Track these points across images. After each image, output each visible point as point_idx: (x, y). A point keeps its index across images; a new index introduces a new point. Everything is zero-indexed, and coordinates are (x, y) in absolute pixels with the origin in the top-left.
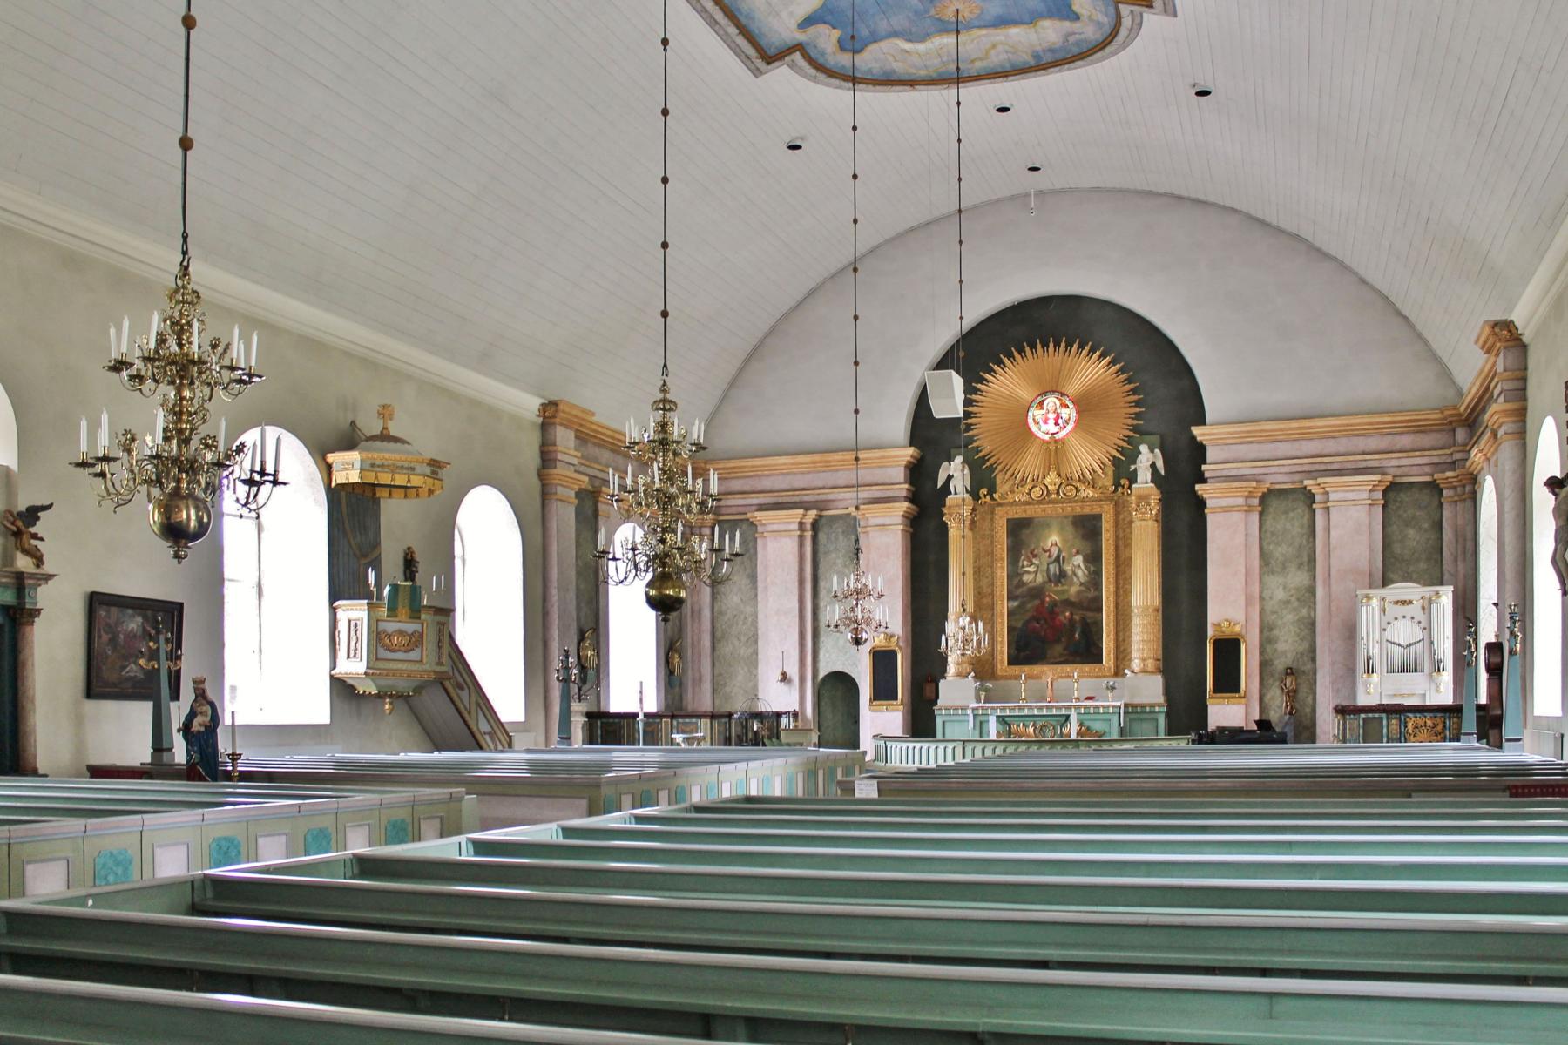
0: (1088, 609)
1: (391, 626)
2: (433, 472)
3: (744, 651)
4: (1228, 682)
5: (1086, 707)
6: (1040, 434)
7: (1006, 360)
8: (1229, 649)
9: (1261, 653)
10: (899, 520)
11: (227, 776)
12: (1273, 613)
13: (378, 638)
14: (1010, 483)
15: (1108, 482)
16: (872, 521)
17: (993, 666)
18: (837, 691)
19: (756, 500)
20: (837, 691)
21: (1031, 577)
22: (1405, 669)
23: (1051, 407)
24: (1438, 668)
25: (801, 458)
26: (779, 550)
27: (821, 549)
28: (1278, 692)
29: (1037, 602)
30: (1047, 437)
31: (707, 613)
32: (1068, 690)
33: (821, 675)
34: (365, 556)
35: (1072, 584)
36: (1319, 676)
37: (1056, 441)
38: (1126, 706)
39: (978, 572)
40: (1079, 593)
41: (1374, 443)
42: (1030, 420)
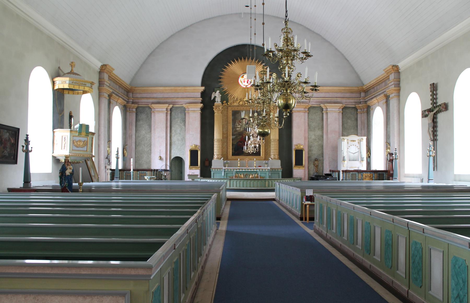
1: (77, 139)
2: (91, 86)
4: (299, 162)
5: (259, 169)
6: (242, 86)
7: (233, 62)
8: (299, 153)
9: (308, 154)
10: (199, 109)
11: (76, 190)
13: (73, 143)
16: (191, 109)
19: (151, 101)
21: (239, 129)
25: (167, 88)
26: (159, 118)
27: (173, 117)
28: (313, 166)
29: (241, 137)
30: (245, 87)
31: (134, 136)
33: (172, 157)
34: (61, 114)
37: (247, 88)
41: (339, 95)
42: (239, 81)
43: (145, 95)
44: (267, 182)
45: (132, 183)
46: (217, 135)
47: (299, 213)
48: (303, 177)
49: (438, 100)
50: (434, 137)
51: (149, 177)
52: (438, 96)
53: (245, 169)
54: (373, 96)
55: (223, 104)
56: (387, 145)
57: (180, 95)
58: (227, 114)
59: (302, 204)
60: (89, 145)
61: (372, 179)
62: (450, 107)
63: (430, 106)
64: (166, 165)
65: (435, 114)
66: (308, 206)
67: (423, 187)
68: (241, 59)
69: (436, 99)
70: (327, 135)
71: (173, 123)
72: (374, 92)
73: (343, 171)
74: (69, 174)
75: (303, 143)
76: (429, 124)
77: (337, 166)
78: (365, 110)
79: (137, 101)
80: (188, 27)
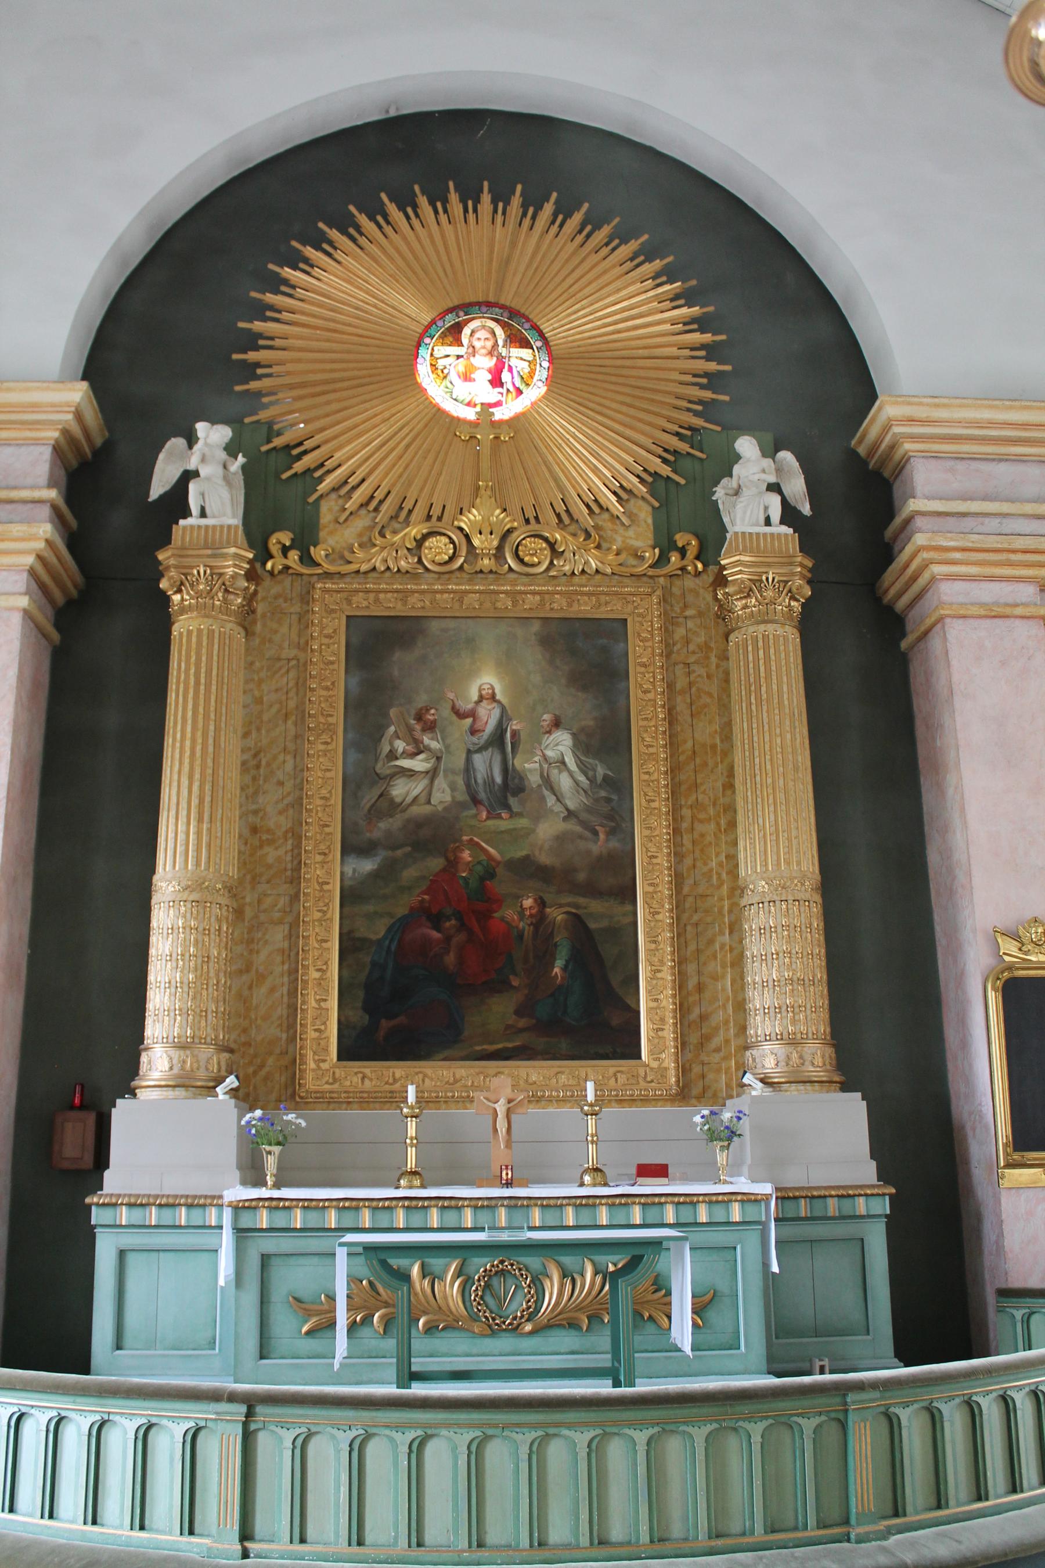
0: (591, 890)
10: (20, 581)
14: (361, 523)
15: (640, 536)
17: (292, 1067)
21: (417, 788)
29: (435, 864)
30: (470, 414)
32: (537, 1144)
35: (540, 814)
37: (495, 424)
38: (785, 1196)
39: (254, 766)
40: (561, 839)
44: (864, 1441)
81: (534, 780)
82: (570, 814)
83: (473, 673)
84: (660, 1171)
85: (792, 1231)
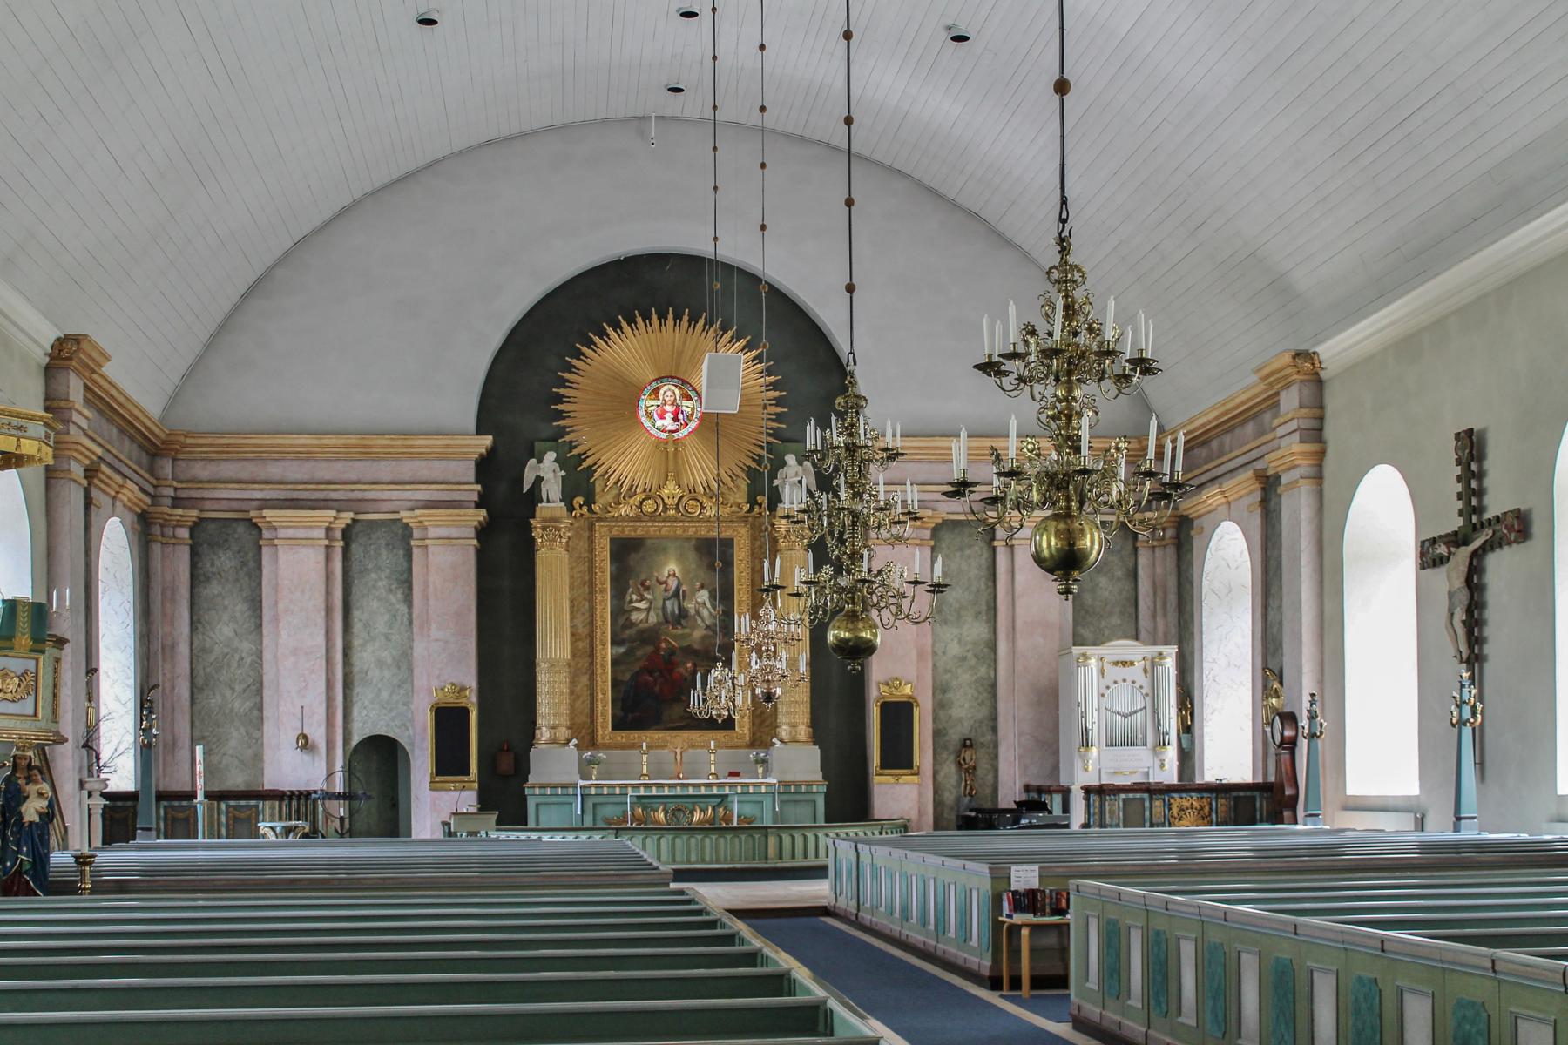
3: (240, 705)
4: (898, 756)
5: (733, 786)
6: (653, 431)
8: (898, 715)
11: (66, 888)
12: (947, 671)
14: (615, 492)
15: (740, 496)
18: (379, 759)
20: (379, 759)
21: (642, 616)
22: (1126, 742)
23: (669, 397)
24: (1161, 743)
25: (327, 440)
26: (297, 566)
27: (355, 567)
29: (650, 649)
30: (663, 436)
31: (183, 649)
33: (356, 740)
35: (694, 627)
36: (1002, 750)
40: (704, 638)
42: (642, 413)
43: (228, 470)
44: (772, 841)
45: (201, 851)
46: (553, 645)
47: (984, 964)
48: (913, 815)
49: (1487, 500)
50: (1471, 648)
51: (279, 825)
52: (1487, 482)
53: (670, 786)
54: (1203, 479)
55: (571, 509)
56: (1265, 679)
57: (385, 470)
58: (592, 551)
59: (997, 925)
60: (44, 693)
61: (1206, 819)
62: (1537, 528)
63: (1456, 523)
64: (330, 775)
65: (1478, 555)
66: (1025, 932)
67: (1427, 848)
68: (647, 317)
69: (1480, 493)
70: (1012, 639)
71: (358, 589)
72: (1208, 460)
73: (1088, 790)
74: (37, 819)
75: (911, 673)
76: (1451, 595)
77: (1056, 768)
78: (1170, 533)
79: (194, 494)
80: (418, 171)
81: (692, 612)
82: (708, 627)
83: (665, 564)
84: (736, 774)
85: (785, 797)
